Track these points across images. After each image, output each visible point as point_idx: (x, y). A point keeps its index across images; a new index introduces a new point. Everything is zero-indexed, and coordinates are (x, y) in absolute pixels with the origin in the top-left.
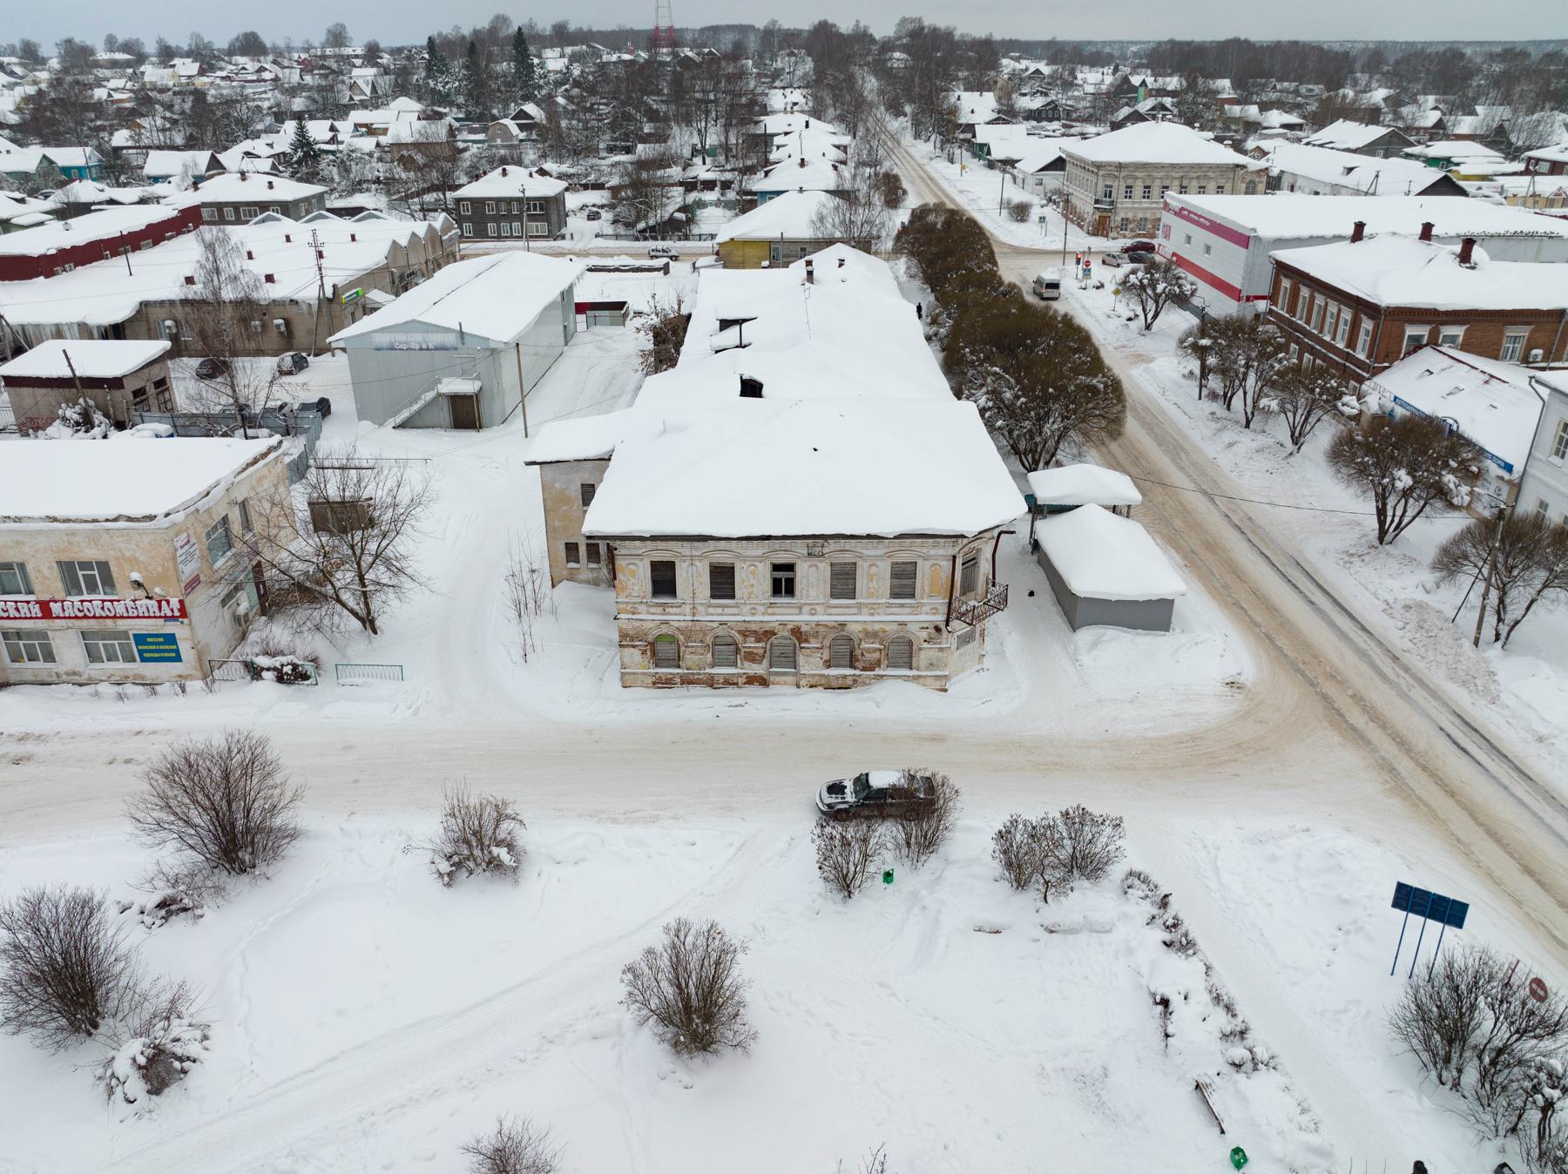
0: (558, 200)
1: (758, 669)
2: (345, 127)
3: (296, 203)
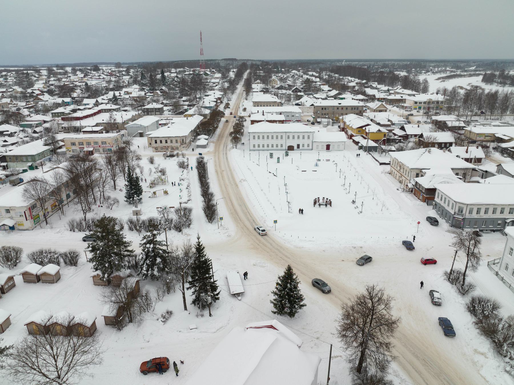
0: (162, 108)
1: (165, 150)
2: (122, 92)
3: (116, 109)
